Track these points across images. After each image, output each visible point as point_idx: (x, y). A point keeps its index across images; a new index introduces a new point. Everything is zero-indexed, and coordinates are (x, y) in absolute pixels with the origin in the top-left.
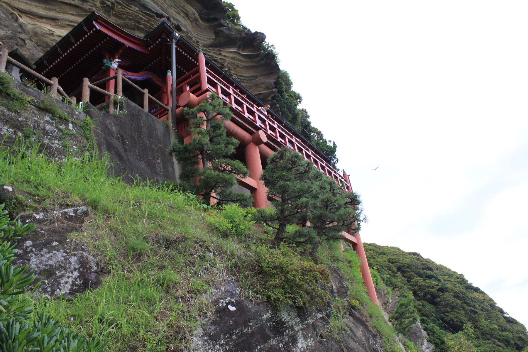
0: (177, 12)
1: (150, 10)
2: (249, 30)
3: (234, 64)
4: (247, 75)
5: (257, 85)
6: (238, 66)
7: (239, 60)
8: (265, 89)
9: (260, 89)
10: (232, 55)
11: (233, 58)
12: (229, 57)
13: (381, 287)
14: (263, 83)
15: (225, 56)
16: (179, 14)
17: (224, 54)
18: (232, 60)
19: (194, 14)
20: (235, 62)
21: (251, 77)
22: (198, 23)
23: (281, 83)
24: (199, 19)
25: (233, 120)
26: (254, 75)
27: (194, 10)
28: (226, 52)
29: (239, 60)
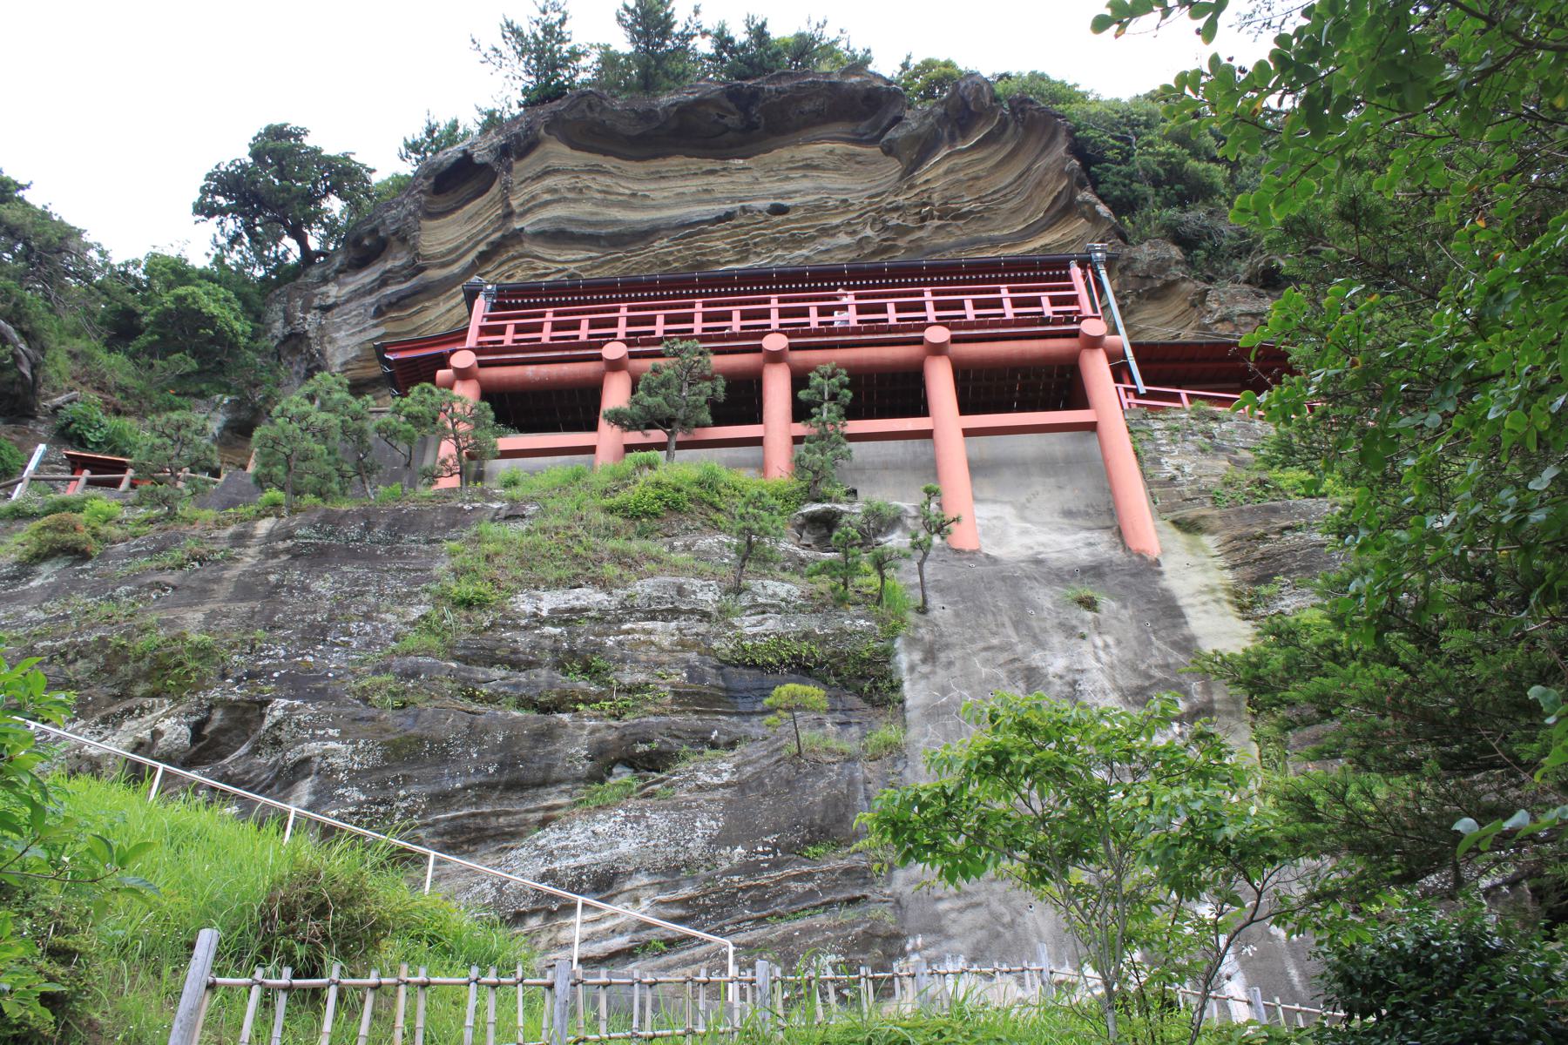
0: (780, 180)
1: (691, 225)
2: (859, 65)
3: (959, 181)
4: (1010, 179)
5: (1039, 184)
6: (977, 178)
7: (970, 164)
8: (1059, 180)
9: (1051, 186)
10: (941, 170)
11: (946, 173)
12: (936, 179)
13: (576, 927)
14: (1047, 170)
15: (927, 181)
16: (787, 179)
17: (919, 181)
18: (951, 177)
19: (831, 152)
20: (961, 175)
21: (1020, 176)
22: (859, 159)
23: (1088, 140)
24: (858, 149)
25: (719, 352)
26: (1023, 167)
27: (828, 146)
28: (928, 171)
29: (970, 164)
